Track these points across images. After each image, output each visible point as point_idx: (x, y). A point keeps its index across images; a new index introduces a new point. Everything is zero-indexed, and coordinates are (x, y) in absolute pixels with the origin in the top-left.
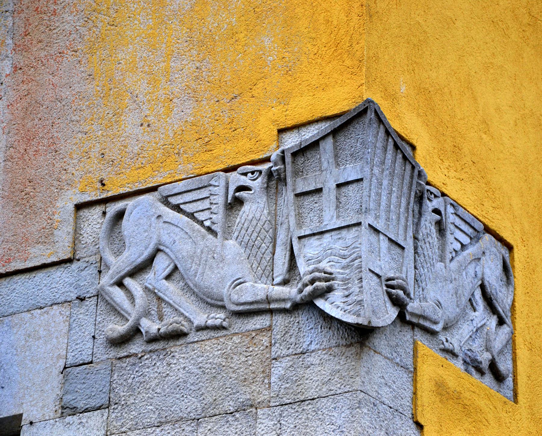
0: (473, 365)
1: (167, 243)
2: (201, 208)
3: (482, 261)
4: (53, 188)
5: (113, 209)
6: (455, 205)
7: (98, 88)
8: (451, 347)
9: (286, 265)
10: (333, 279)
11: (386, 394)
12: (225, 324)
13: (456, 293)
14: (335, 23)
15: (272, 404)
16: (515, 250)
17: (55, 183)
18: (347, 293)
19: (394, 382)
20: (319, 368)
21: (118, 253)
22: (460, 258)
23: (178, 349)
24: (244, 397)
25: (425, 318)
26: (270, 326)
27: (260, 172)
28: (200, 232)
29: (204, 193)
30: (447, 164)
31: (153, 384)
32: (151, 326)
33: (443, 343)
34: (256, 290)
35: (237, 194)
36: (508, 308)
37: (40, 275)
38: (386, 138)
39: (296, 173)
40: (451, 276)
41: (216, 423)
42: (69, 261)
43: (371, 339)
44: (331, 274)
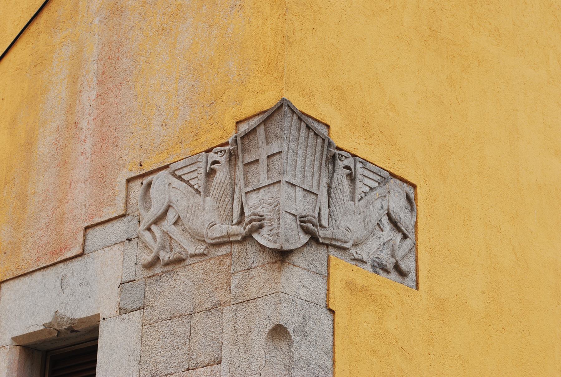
0: (380, 267)
1: (174, 202)
2: (193, 177)
3: (387, 198)
4: (115, 170)
5: (146, 180)
6: (364, 162)
7: (140, 104)
8: (360, 257)
9: (239, 212)
10: (264, 219)
11: (303, 293)
12: (205, 252)
13: (364, 221)
14: (268, 49)
15: (231, 303)
16: (418, 187)
17: (117, 166)
18: (271, 228)
19: (311, 284)
20: (257, 279)
21: (148, 210)
22: (368, 197)
23: (180, 269)
24: (216, 299)
25: (336, 240)
26: (231, 252)
27: (225, 151)
28: (191, 192)
29: (194, 167)
30: (357, 135)
31: (167, 293)
32: (165, 256)
33: (353, 255)
34: (222, 229)
35: (212, 166)
36: (411, 227)
37: (109, 225)
38: (299, 123)
39: (244, 151)
40: (360, 210)
41: (201, 316)
42: (123, 216)
43: (290, 257)
44: (262, 216)
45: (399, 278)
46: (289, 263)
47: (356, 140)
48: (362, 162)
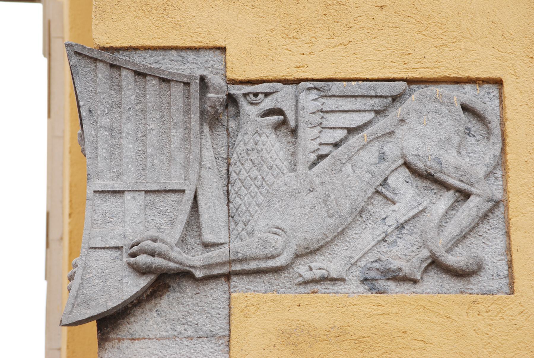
46: (119, 340)
47: (305, 49)
48: (315, 88)
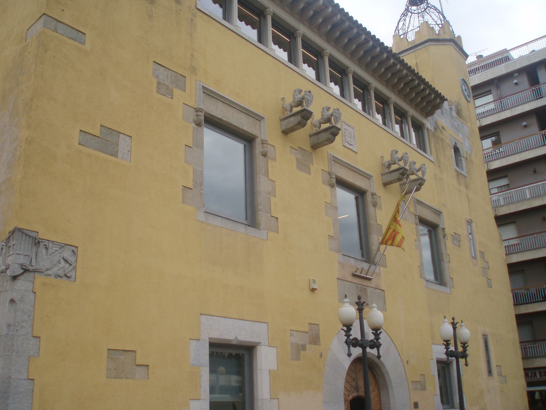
0: (58, 276)
45: (67, 279)
